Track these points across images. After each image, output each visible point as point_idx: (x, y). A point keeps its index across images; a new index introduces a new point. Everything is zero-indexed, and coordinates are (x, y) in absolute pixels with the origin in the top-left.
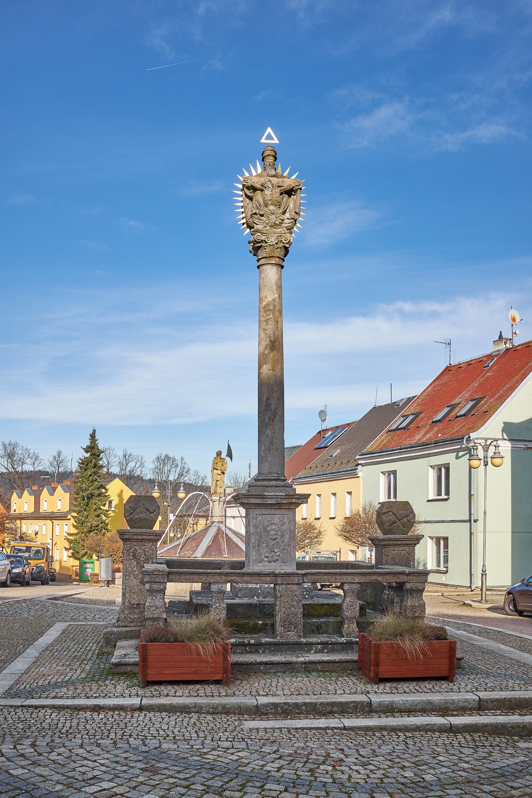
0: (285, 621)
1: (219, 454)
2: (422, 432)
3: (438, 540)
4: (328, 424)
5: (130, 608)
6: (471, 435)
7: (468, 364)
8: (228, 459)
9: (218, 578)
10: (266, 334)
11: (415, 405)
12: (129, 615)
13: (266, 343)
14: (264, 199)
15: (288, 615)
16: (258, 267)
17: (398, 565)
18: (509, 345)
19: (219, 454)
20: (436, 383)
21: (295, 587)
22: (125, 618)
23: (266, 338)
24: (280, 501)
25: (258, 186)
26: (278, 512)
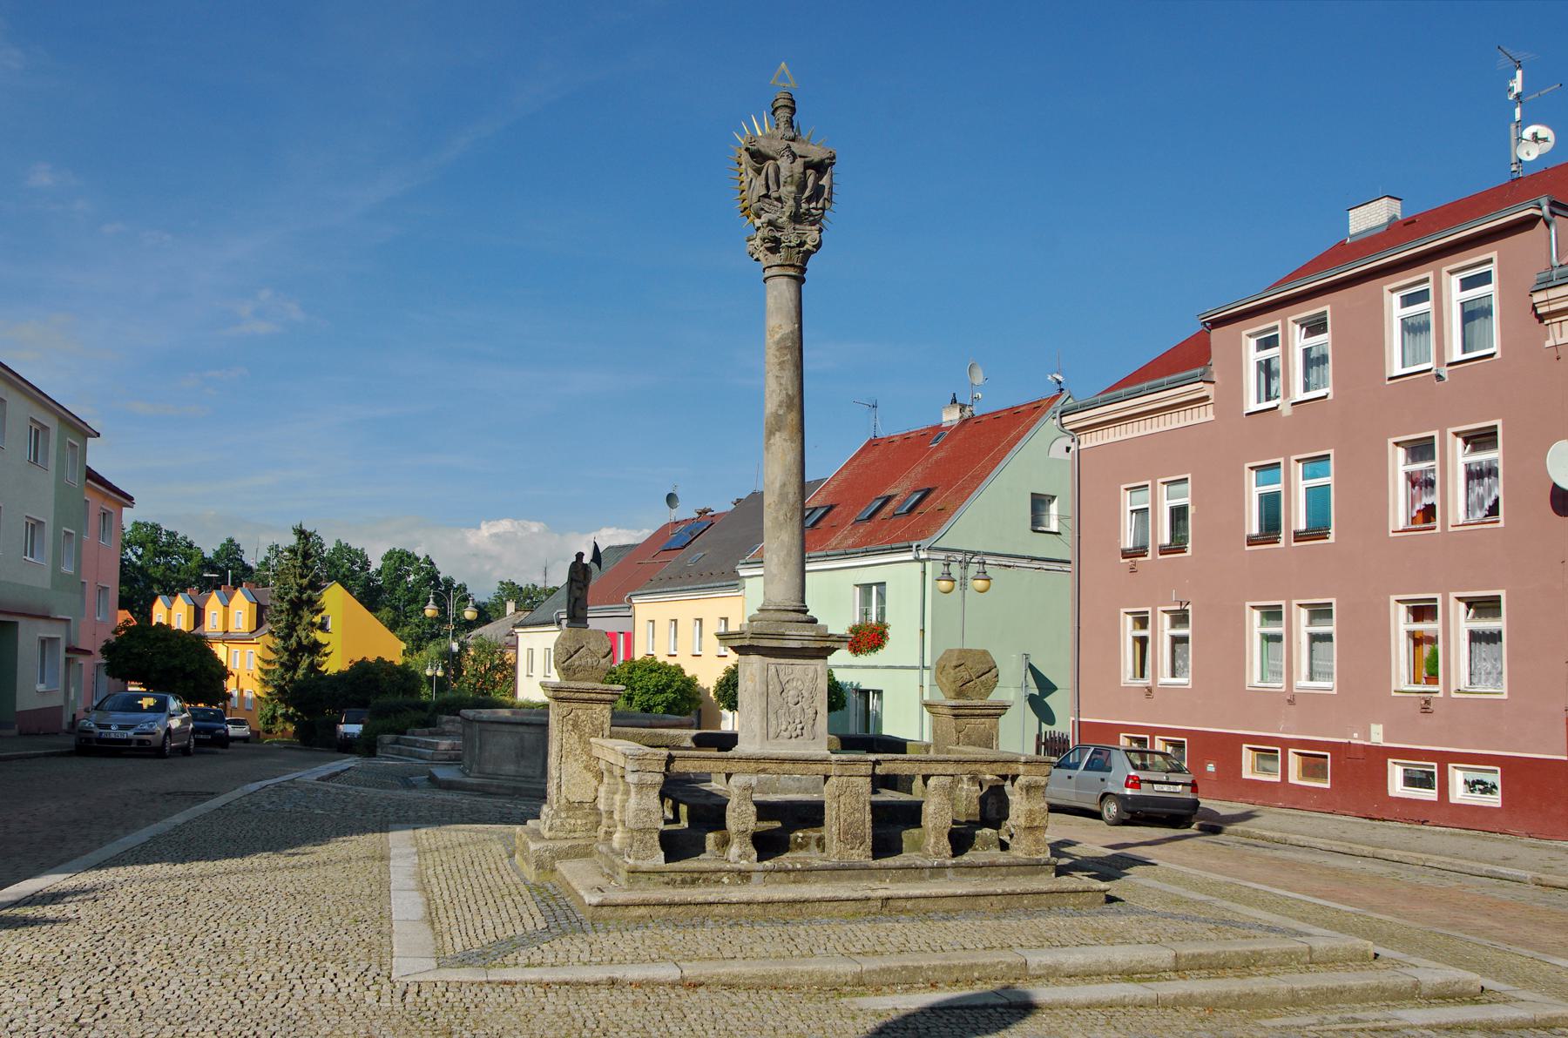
1: (580, 556)
2: (839, 536)
5: (568, 809)
7: (906, 438)
8: (594, 566)
9: (744, 765)
11: (823, 493)
19: (580, 556)
21: (861, 781)
24: (807, 644)
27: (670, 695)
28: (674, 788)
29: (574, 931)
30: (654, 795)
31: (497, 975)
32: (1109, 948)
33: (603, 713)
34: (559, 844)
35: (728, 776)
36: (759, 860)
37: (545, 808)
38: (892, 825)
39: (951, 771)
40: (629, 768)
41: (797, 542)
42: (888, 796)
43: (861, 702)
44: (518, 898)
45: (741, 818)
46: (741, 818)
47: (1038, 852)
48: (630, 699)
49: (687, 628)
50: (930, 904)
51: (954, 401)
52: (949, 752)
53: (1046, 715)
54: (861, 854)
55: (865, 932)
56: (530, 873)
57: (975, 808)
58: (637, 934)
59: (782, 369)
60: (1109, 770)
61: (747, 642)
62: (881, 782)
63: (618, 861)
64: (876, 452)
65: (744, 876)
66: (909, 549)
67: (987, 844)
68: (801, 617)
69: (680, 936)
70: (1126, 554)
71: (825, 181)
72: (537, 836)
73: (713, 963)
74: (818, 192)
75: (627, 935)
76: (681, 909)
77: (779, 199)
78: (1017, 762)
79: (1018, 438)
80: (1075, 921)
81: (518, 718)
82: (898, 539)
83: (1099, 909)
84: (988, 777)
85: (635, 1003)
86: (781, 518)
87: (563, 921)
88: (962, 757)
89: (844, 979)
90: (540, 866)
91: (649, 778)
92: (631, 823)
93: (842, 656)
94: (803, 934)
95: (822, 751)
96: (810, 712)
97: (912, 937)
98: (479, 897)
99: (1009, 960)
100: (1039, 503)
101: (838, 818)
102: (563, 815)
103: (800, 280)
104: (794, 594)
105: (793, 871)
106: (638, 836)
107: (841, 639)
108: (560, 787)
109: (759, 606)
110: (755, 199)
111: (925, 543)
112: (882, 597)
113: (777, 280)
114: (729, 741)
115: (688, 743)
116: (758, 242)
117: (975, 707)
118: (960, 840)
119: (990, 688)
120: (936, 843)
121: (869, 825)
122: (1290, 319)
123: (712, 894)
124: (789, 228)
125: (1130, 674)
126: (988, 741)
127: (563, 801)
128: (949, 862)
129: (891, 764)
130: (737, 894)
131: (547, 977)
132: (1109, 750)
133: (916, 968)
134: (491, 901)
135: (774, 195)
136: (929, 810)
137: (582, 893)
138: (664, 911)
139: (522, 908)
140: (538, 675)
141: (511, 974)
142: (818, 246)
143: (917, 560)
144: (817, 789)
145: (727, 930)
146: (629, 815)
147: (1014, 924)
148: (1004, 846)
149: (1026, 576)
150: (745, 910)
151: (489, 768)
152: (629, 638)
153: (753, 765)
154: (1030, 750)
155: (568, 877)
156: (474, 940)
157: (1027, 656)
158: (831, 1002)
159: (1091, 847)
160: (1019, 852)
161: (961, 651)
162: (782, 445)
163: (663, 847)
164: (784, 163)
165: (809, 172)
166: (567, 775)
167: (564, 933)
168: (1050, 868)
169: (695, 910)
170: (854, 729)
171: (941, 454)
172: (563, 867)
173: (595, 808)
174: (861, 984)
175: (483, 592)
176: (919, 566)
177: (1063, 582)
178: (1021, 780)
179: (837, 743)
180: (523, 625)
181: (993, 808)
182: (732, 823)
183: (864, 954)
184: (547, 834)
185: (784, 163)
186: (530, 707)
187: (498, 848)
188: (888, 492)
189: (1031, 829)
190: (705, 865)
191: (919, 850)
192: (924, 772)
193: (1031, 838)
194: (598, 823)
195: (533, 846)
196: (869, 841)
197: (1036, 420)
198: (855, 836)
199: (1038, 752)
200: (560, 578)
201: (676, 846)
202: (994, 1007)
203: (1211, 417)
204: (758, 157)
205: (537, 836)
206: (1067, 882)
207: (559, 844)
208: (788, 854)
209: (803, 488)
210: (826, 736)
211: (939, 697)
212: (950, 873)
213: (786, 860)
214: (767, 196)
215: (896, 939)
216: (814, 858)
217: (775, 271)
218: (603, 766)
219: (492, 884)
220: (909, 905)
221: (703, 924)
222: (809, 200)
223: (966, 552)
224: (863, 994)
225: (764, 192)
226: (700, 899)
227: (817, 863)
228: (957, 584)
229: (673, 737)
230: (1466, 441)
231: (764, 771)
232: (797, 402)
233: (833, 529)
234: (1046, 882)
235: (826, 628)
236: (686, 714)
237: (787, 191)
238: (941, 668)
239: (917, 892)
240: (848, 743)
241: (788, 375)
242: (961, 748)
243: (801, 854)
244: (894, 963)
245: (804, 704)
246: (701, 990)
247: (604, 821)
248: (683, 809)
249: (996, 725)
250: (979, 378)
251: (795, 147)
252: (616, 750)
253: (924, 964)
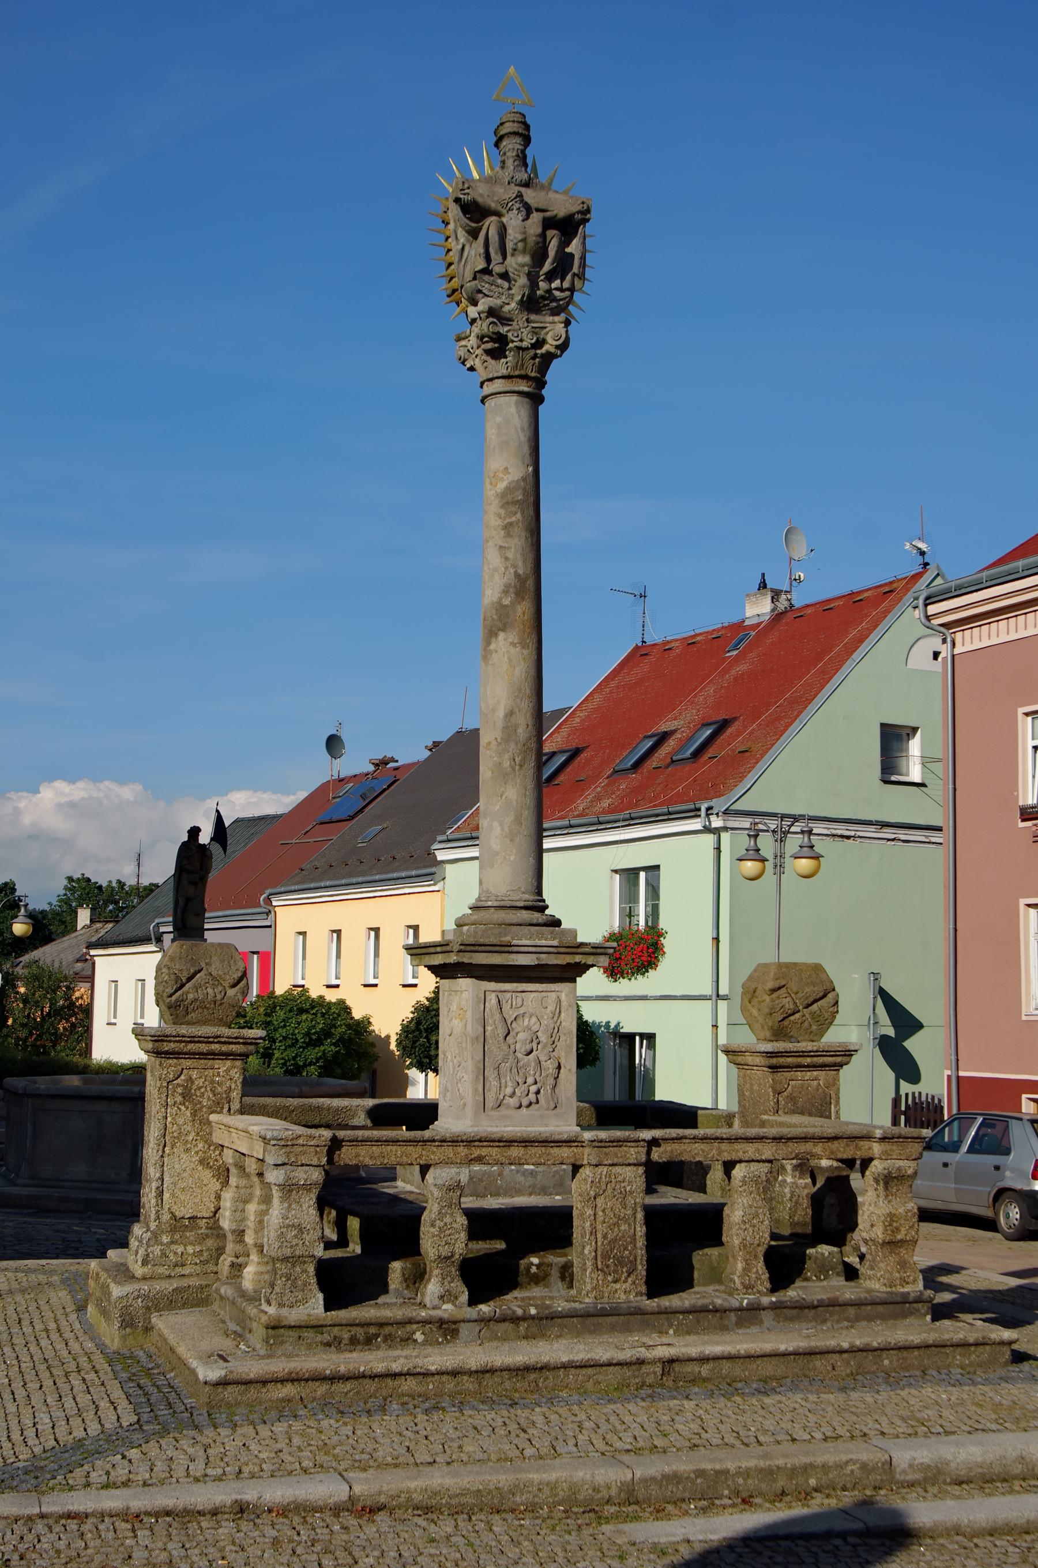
1: (194, 832)
2: (589, 795)
5: (173, 1230)
7: (689, 643)
8: (216, 849)
9: (448, 1151)
10: (507, 559)
11: (565, 731)
12: (174, 1247)
13: (505, 580)
15: (615, 1240)
16: (483, 401)
17: (802, 1113)
19: (194, 832)
20: (613, 684)
21: (628, 1172)
22: (164, 1255)
23: (506, 568)
24: (545, 959)
27: (328, 1048)
28: (343, 1191)
29: (181, 1427)
30: (309, 1201)
31: (55, 1503)
32: (1021, 1435)
33: (229, 1075)
34: (158, 1286)
35: (424, 1169)
36: (472, 1302)
37: (137, 1230)
38: (676, 1242)
39: (767, 1154)
40: (270, 1160)
41: (530, 801)
42: (670, 1196)
43: (622, 1052)
44: (91, 1376)
45: (442, 1236)
46: (442, 1236)
47: (904, 1282)
48: (267, 1056)
49: (356, 942)
50: (737, 1370)
51: (763, 585)
52: (763, 1124)
53: (905, 1068)
54: (628, 1291)
55: (636, 1416)
56: (111, 1334)
57: (804, 1213)
58: (280, 1428)
59: (508, 535)
60: (1007, 1152)
61: (453, 958)
62: (660, 1174)
63: (251, 1311)
64: (644, 667)
65: (447, 1329)
66: (695, 813)
67: (824, 1270)
68: (536, 916)
69: (347, 1430)
71: (574, 247)
72: (123, 1273)
73: (400, 1472)
74: (563, 265)
75: (264, 1431)
76: (349, 1385)
77: (505, 276)
78: (868, 1137)
79: (861, 640)
80: (965, 1392)
81: (94, 1089)
82: (679, 799)
83: (1001, 1372)
84: (825, 1163)
85: (276, 1543)
86: (507, 764)
87: (163, 1412)
88: (784, 1131)
89: (605, 1494)
90: (127, 1322)
91: (301, 1175)
92: (272, 1248)
93: (593, 981)
94: (540, 1420)
95: (565, 1125)
96: (550, 1066)
97: (710, 1421)
98: (30, 1376)
99: (864, 1457)
100: (893, 738)
101: (594, 1232)
102: (165, 1239)
103: (536, 399)
104: (525, 882)
105: (524, 1318)
106: (282, 1268)
107: (596, 950)
108: (160, 1194)
109: (472, 901)
110: (468, 276)
111: (720, 804)
112: (654, 891)
113: (502, 399)
114: (425, 1114)
115: (361, 1119)
116: (473, 341)
117: (803, 1054)
118: (784, 1263)
119: (826, 1021)
120: (746, 1270)
121: (641, 1242)
123: (398, 1359)
124: (520, 320)
126: (824, 1105)
127: (166, 1217)
128: (765, 1300)
129: (675, 1146)
130: (438, 1358)
131: (137, 1504)
132: (1005, 1121)
133: (718, 1473)
134: (48, 1383)
135: (498, 269)
136: (734, 1216)
137: (194, 1363)
138: (322, 1389)
139: (97, 1392)
140: (126, 1021)
141: (79, 1502)
142: (564, 347)
143: (707, 830)
144: (561, 1187)
145: (421, 1418)
146: (270, 1235)
147: (869, 1398)
148: (851, 1273)
149: (873, 853)
150: (450, 1384)
152: (267, 960)
153: (462, 1151)
154: (883, 1118)
155: (172, 1339)
156: (20, 1448)
157: (876, 976)
158: (586, 1532)
159: (981, 1274)
160: (875, 1282)
161: (780, 966)
162: (508, 653)
163: (322, 1286)
164: (513, 220)
165: (551, 233)
166: (173, 1176)
167: (165, 1431)
168: (923, 1308)
169: (371, 1386)
170: (612, 1093)
171: (742, 667)
172: (163, 1323)
173: (215, 1227)
174: (633, 1501)
175: (41, 892)
176: (710, 839)
177: (929, 860)
178: (877, 1167)
179: (590, 1115)
180: (103, 944)
181: (833, 1211)
182: (430, 1245)
183: (637, 1451)
184: (139, 1271)
185: (513, 220)
186: (111, 1071)
187: (62, 1297)
188: (664, 727)
189: (892, 1244)
190: (387, 1313)
191: (720, 1282)
192: (726, 1157)
193: (893, 1259)
194: (220, 1251)
195: (117, 1291)
196: (641, 1269)
197: (887, 612)
198: (620, 1262)
199: (895, 1122)
200: (160, 868)
201: (344, 1283)
202: (843, 1535)
204: (474, 212)
205: (123, 1273)
206: (951, 1330)
207: (158, 1286)
208: (516, 1293)
209: (539, 719)
210: (575, 1104)
211: (746, 1038)
212: (767, 1317)
213: (513, 1301)
214: (487, 271)
215: (686, 1426)
216: (557, 1298)
217: (498, 385)
218: (228, 1157)
219: (50, 1354)
220: (705, 1370)
221: (383, 1409)
222: (550, 277)
223: (783, 817)
224: (636, 1518)
225: (481, 265)
226: (380, 1368)
227: (561, 1306)
228: (769, 865)
229: (338, 1111)
231: (479, 1160)
232: (530, 586)
233: (580, 785)
234: (916, 1330)
235: (574, 933)
236: (353, 1078)
237: (517, 262)
238: (750, 994)
239: (717, 1349)
240: (606, 1115)
241: (518, 543)
242: (783, 1118)
243: (536, 1292)
244: (684, 1465)
245: (541, 1053)
246: (381, 1517)
247: (230, 1247)
248: (354, 1224)
249: (836, 1079)
250: (800, 550)
251: (530, 196)
252: (247, 1132)
253: (731, 1466)
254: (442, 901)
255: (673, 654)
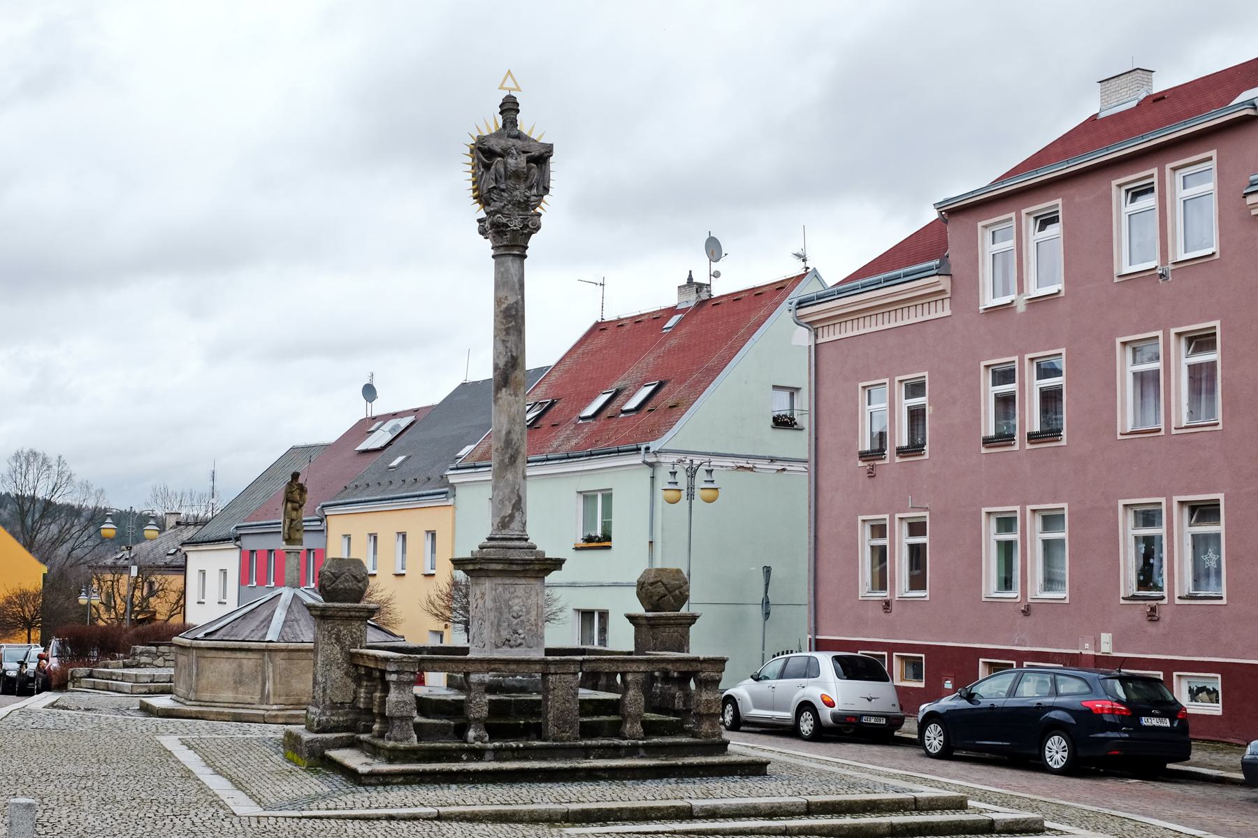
0: (558, 719)
3: (587, 615)
4: (379, 408)
6: (651, 444)
7: (637, 320)
9: (479, 666)
11: (544, 387)
14: (506, 168)
18: (704, 296)
20: (580, 351)
21: (570, 678)
25: (498, 149)
26: (523, 581)
49: (389, 543)
59: (508, 334)
64: (602, 340)
70: (863, 456)
122: (1024, 212)
125: (994, 584)
151: (206, 696)
171: (673, 342)
203: (948, 312)
228: (684, 493)
230: (1190, 340)
254: (454, 513)
255: (624, 329)
